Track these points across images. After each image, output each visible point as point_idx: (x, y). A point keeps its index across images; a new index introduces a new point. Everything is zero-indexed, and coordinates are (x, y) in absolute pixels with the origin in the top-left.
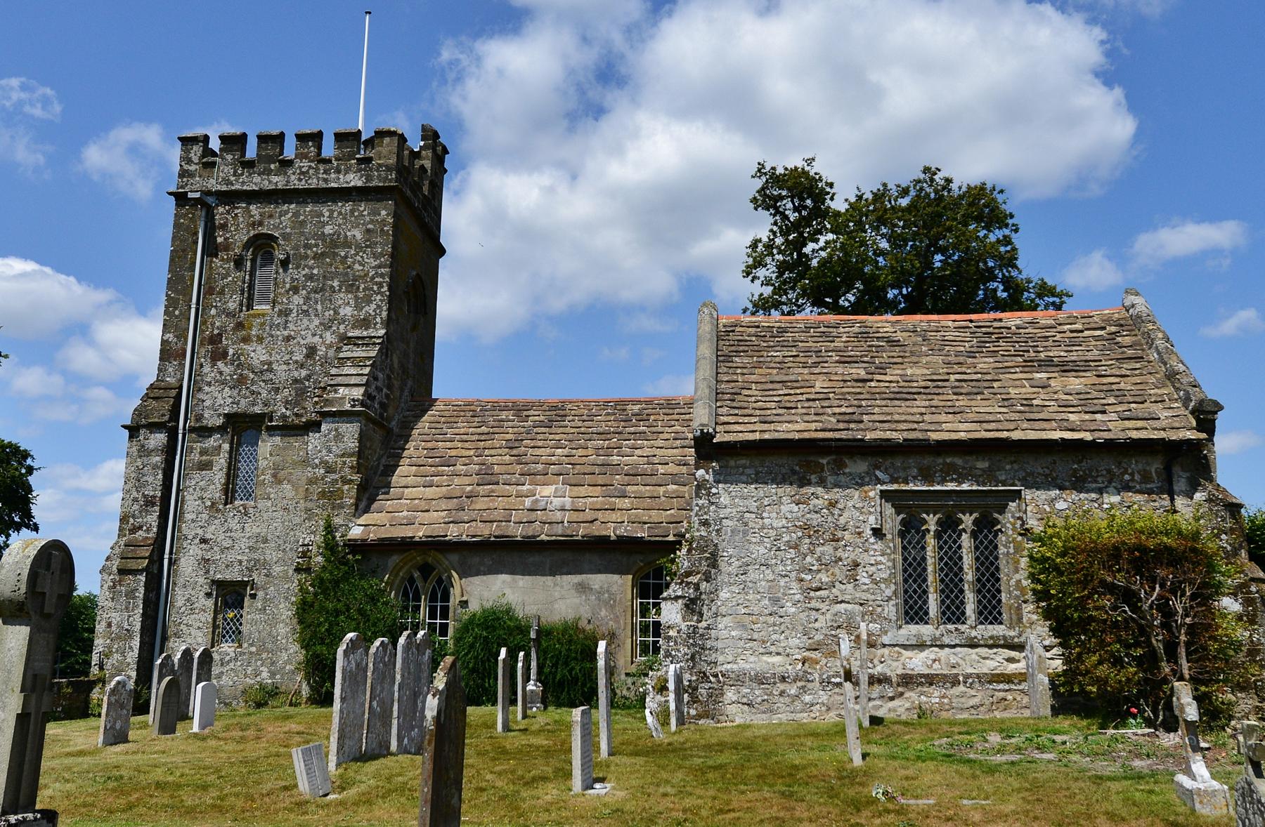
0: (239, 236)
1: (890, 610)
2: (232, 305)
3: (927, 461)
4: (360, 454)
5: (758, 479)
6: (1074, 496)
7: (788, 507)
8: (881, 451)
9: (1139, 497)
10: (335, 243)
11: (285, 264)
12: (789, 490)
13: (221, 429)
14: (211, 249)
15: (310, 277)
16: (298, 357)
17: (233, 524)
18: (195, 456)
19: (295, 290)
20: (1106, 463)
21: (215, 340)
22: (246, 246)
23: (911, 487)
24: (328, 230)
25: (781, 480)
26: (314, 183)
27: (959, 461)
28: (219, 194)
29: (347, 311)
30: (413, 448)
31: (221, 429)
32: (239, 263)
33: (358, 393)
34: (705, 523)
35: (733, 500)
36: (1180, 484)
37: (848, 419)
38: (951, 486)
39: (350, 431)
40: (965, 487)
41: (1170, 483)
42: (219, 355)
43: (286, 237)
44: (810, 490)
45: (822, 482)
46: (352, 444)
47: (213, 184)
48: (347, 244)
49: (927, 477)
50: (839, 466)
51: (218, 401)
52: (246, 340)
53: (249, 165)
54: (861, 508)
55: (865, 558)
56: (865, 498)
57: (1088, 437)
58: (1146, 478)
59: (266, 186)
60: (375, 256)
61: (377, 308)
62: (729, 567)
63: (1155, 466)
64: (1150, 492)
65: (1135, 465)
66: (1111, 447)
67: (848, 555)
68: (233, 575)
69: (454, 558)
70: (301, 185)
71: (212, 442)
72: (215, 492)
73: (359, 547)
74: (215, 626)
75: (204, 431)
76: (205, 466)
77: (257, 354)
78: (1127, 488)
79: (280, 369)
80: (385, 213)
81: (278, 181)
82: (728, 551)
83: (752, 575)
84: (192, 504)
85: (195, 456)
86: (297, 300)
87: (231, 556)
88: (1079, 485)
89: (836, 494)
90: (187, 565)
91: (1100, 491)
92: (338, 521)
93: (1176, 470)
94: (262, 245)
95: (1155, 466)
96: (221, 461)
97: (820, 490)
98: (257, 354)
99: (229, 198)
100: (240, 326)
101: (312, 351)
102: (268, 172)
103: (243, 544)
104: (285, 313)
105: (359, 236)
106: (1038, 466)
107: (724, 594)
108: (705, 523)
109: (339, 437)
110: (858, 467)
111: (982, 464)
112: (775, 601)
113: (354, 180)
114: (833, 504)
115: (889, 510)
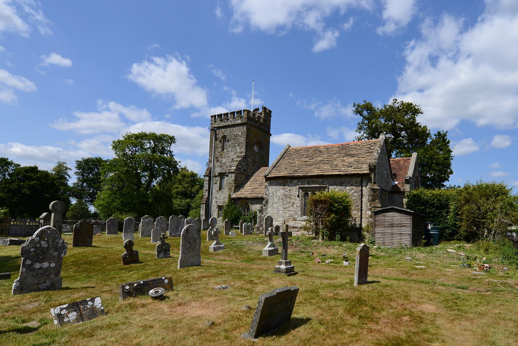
0: (220, 136)
1: (299, 213)
2: (220, 151)
3: (309, 180)
4: (235, 180)
5: (276, 185)
6: (339, 187)
7: (282, 191)
8: (299, 178)
9: (354, 187)
10: (237, 136)
11: (228, 141)
12: (282, 187)
13: (218, 176)
14: (216, 139)
15: (232, 144)
16: (230, 161)
17: (220, 194)
18: (214, 181)
19: (230, 146)
20: (347, 179)
21: (217, 158)
22: (222, 138)
23: (305, 186)
24: (235, 133)
25: (280, 185)
26: (233, 123)
27: (315, 180)
28: (217, 127)
29: (238, 150)
30: (252, 179)
31: (218, 176)
32: (220, 141)
33: (235, 168)
34: (266, 194)
35: (272, 189)
36: (364, 184)
37: (296, 171)
38: (314, 186)
39: (233, 175)
40: (316, 186)
41: (362, 183)
42: (218, 161)
43: (228, 135)
44: (286, 187)
45: (288, 185)
46: (234, 178)
47: (216, 126)
48: (238, 136)
49: (309, 184)
50: (287, 182)
51: (218, 170)
52: (222, 158)
53: (222, 121)
54: (294, 190)
55: (296, 202)
56: (296, 189)
57: (341, 173)
58: (357, 183)
59: (225, 125)
60: (243, 138)
61: (243, 149)
62: (270, 204)
63: (359, 180)
64: (357, 186)
65: (354, 180)
66: (346, 175)
67: (292, 201)
68: (220, 204)
69: (250, 201)
70: (230, 124)
71: (217, 178)
72: (218, 189)
73: (234, 199)
74: (218, 214)
75: (216, 176)
76: (216, 183)
77: (224, 160)
78: (352, 185)
79: (227, 163)
80: (245, 128)
81: (227, 124)
82: (270, 200)
83: (274, 205)
84: (214, 191)
85: (214, 181)
86: (230, 149)
87: (220, 201)
88: (341, 185)
89: (291, 188)
90: (214, 202)
91: (346, 186)
92: (231, 194)
93: (364, 181)
94: (224, 137)
95: (359, 180)
96: (219, 182)
97: (288, 187)
98: (224, 160)
99: (219, 128)
100: (221, 155)
101: (233, 159)
102: (225, 122)
103: (222, 198)
104: (228, 151)
105: (240, 133)
106: (332, 180)
107: (269, 209)
108: (266, 194)
109: (231, 177)
110: (295, 182)
111: (320, 180)
112: (278, 211)
113: (239, 122)
114: (290, 190)
115: (301, 191)
